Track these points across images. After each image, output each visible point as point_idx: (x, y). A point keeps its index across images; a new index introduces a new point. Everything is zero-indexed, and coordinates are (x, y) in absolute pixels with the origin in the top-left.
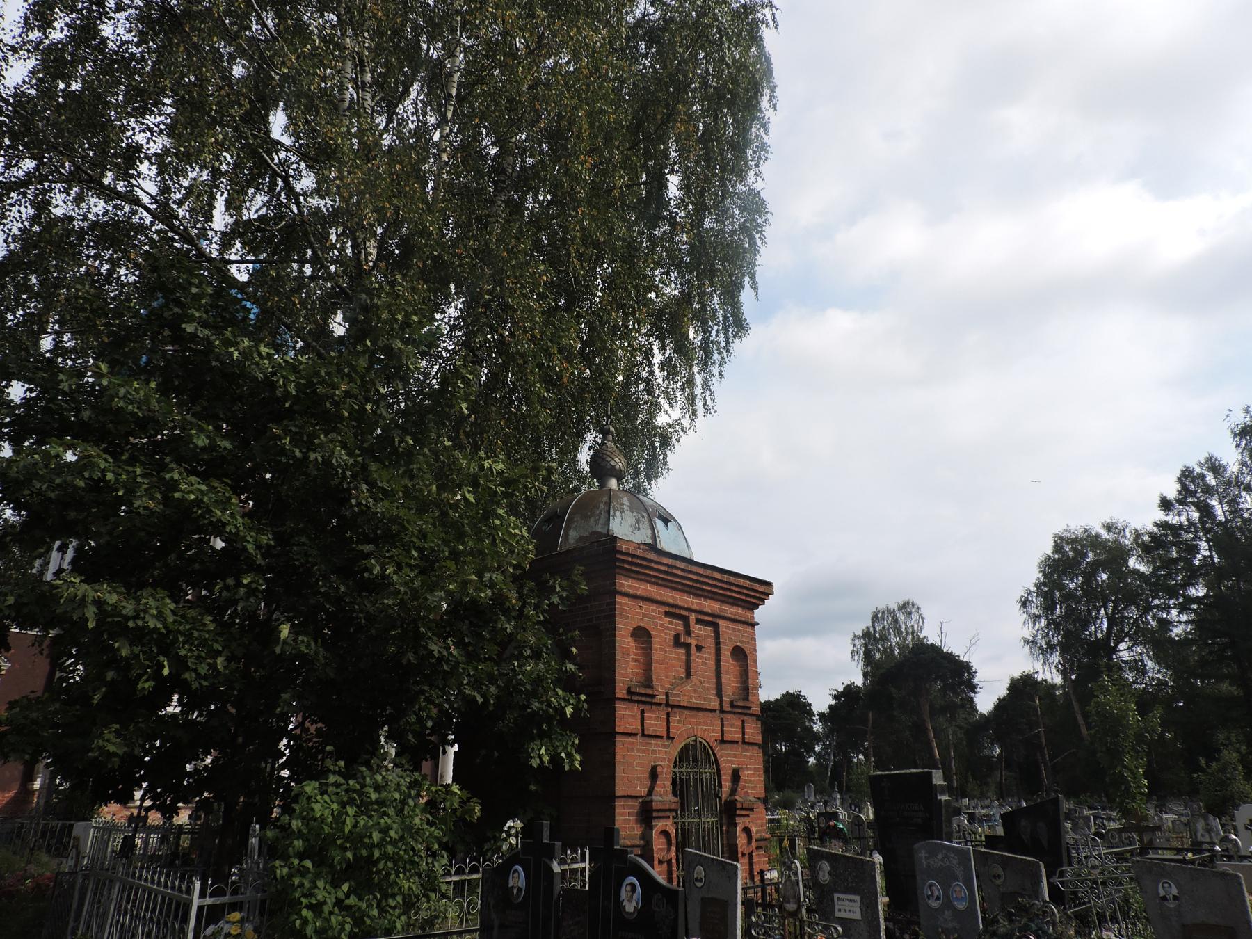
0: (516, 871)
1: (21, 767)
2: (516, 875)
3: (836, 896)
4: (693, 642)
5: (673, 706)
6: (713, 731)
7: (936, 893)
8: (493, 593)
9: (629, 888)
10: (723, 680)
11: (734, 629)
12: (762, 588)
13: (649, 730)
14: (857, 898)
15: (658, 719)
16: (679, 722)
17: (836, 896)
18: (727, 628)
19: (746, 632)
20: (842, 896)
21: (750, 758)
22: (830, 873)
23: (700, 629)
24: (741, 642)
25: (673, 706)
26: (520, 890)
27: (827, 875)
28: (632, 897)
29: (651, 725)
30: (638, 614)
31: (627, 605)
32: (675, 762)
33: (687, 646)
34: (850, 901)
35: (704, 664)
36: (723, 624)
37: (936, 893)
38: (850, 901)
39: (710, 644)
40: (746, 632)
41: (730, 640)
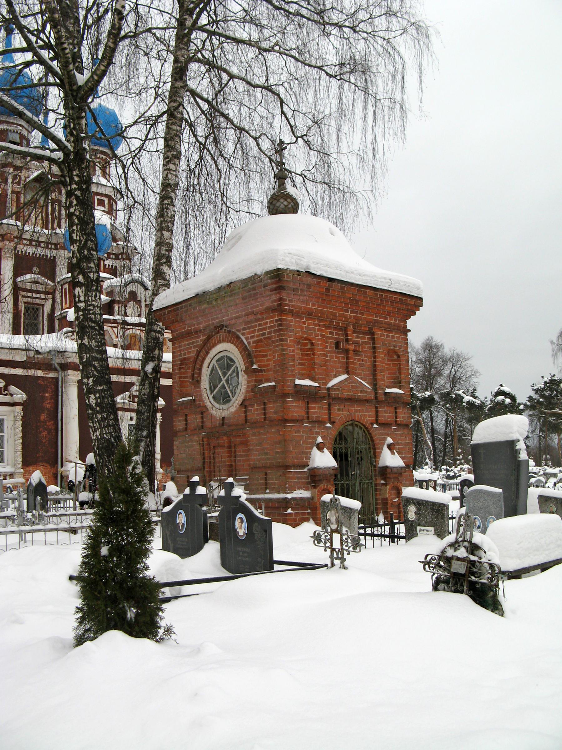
0: (180, 513)
1: (463, 573)
2: (180, 516)
3: (419, 528)
4: (351, 347)
5: (334, 399)
6: (369, 416)
7: (478, 524)
8: (34, 357)
9: (239, 520)
10: (379, 377)
11: (387, 336)
12: (413, 302)
13: (313, 416)
14: (432, 529)
15: (320, 408)
16: (339, 410)
17: (419, 528)
18: (381, 335)
19: (398, 338)
20: (422, 528)
21: (401, 435)
22: (415, 513)
23: (358, 337)
24: (394, 346)
25: (334, 399)
26: (183, 525)
27: (414, 514)
28: (241, 526)
29: (314, 413)
30: (302, 328)
31: (292, 321)
32: (336, 440)
33: (347, 351)
34: (427, 531)
35: (361, 365)
36: (378, 333)
37: (478, 524)
38: (427, 531)
39: (367, 349)
40: (398, 338)
41: (385, 345)
